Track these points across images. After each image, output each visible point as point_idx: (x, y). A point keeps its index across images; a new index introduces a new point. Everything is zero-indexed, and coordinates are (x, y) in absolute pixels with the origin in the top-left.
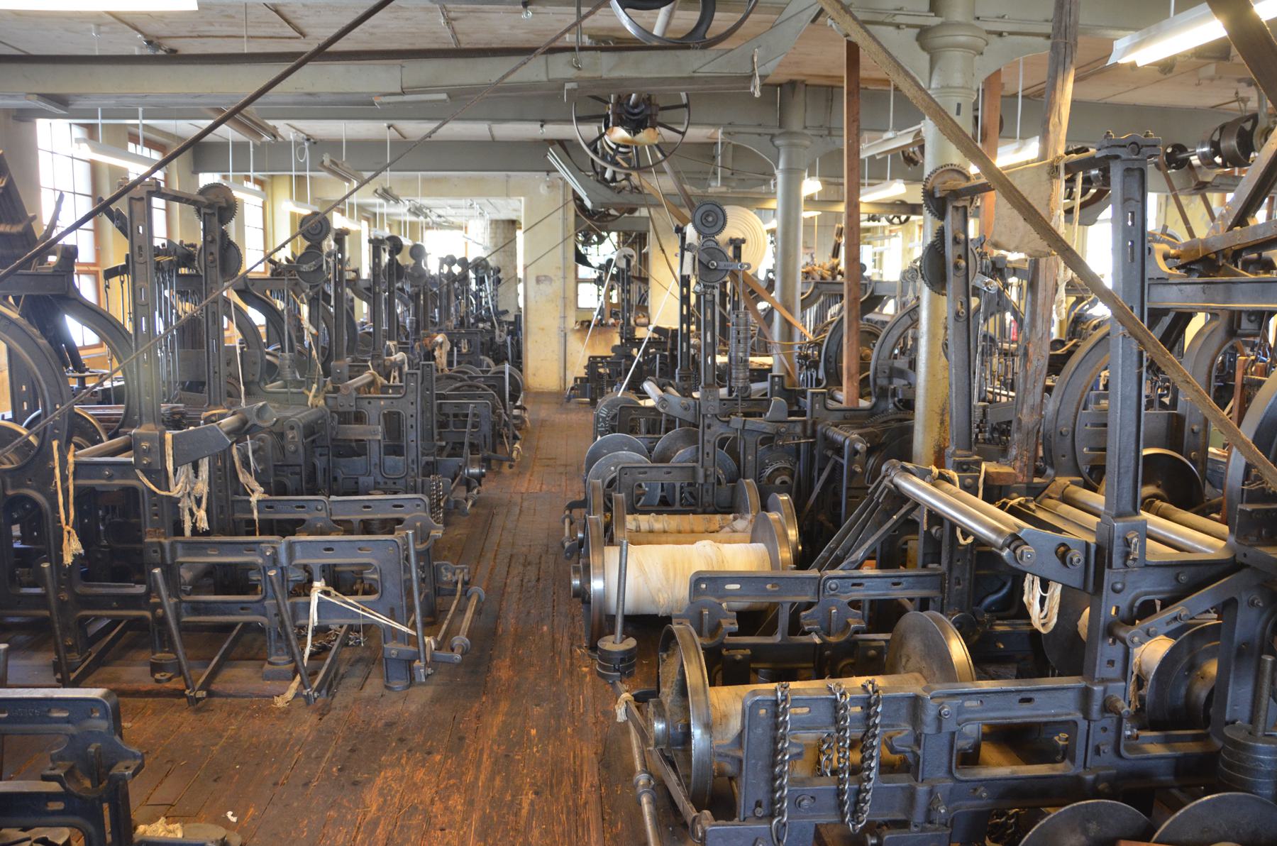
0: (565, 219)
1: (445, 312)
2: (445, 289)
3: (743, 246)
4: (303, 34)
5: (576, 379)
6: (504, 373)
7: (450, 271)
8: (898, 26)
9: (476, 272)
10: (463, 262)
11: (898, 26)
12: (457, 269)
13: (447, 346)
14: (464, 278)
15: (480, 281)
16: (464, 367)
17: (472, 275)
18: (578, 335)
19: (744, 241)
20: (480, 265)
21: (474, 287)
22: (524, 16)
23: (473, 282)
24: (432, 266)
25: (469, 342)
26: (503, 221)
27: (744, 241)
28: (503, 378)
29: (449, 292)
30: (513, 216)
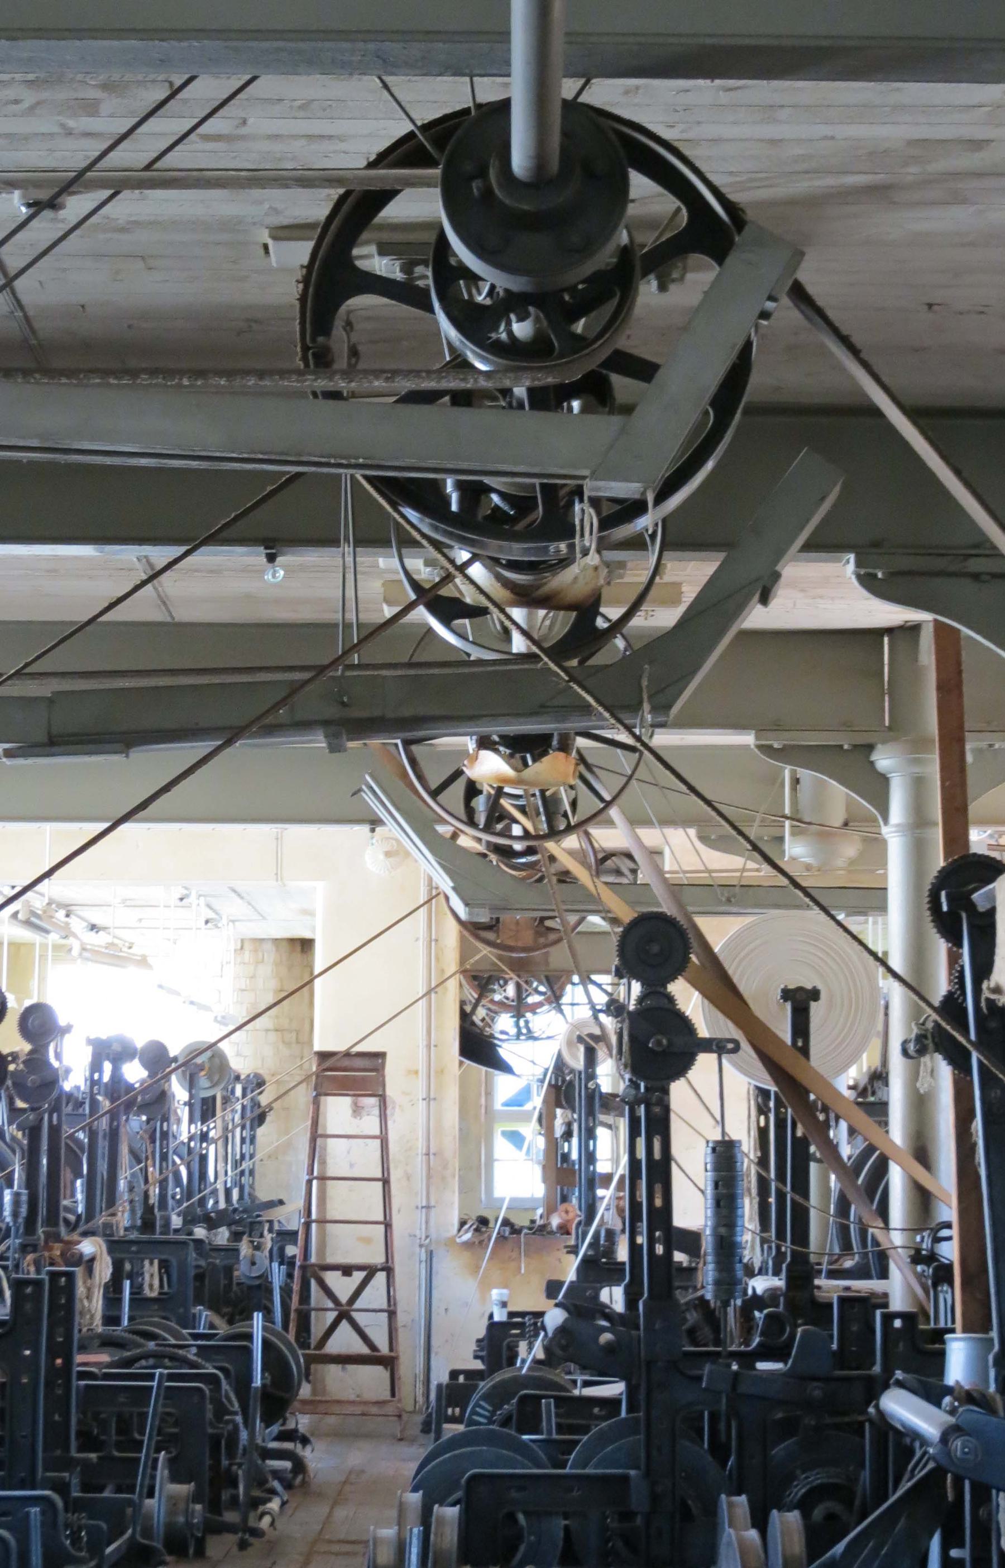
0: (433, 941)
1: (103, 1192)
2: (104, 1123)
3: (813, 1005)
4: (264, 918)
5: (454, 1374)
6: (249, 1337)
7: (116, 1076)
8: (976, 577)
9: (191, 1084)
10: (157, 1059)
11: (976, 577)
12: (134, 1073)
13: (104, 1270)
14: (155, 1102)
15: (205, 1110)
16: (153, 1322)
17: (179, 1092)
18: (467, 1255)
19: (815, 994)
20: (204, 1064)
21: (184, 1129)
22: (268, 577)
23: (184, 1113)
24: (73, 1065)
25: (164, 1265)
26: (276, 941)
27: (815, 994)
28: (248, 1352)
29: (114, 1136)
30: (307, 935)
